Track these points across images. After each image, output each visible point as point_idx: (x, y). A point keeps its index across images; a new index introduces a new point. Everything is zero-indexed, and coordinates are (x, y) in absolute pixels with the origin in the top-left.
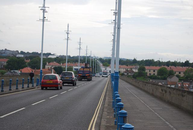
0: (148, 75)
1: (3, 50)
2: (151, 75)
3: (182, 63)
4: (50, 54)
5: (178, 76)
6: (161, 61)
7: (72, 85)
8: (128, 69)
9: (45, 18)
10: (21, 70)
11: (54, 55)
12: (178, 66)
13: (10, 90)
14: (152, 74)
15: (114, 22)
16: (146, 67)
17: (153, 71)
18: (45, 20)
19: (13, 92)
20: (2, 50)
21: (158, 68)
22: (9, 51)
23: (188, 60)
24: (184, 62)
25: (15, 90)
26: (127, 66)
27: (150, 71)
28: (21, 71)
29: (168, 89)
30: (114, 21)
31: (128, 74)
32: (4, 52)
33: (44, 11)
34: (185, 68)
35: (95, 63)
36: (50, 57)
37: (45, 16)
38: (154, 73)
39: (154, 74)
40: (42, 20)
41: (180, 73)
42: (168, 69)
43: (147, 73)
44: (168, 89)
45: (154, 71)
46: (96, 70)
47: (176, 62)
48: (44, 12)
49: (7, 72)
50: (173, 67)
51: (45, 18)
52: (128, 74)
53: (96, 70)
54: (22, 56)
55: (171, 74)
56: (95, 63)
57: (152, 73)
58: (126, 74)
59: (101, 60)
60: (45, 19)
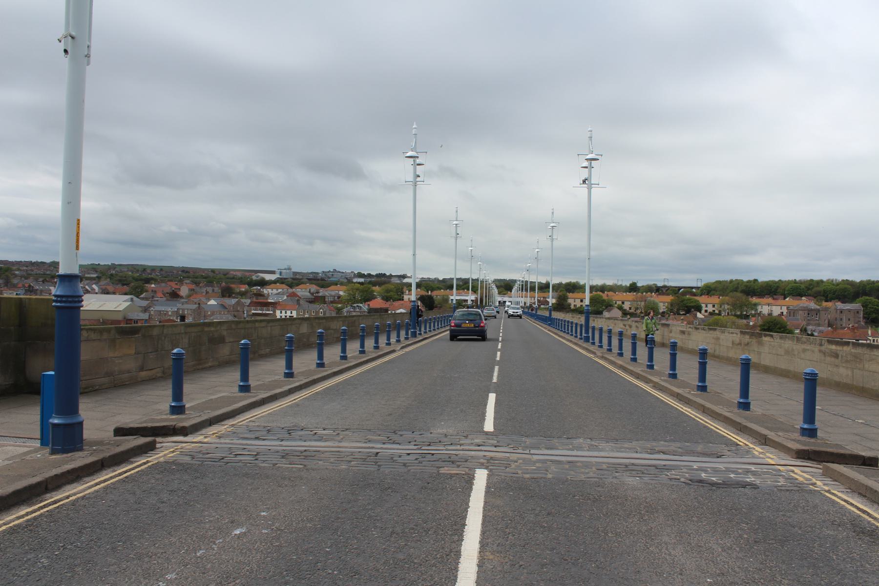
0: (572, 307)
1: (330, 272)
2: (577, 306)
5: (620, 308)
9: (458, 234)
14: (578, 306)
15: (550, 238)
17: (579, 300)
20: (328, 272)
22: (339, 272)
24: (628, 285)
27: (575, 302)
28: (369, 305)
29: (634, 323)
30: (550, 236)
33: (552, 240)
34: (631, 296)
37: (458, 233)
41: (623, 303)
42: (604, 296)
43: (570, 305)
44: (634, 323)
46: (489, 299)
47: (616, 285)
49: (347, 307)
50: (611, 293)
51: (458, 234)
53: (489, 299)
54: (362, 280)
55: (609, 306)
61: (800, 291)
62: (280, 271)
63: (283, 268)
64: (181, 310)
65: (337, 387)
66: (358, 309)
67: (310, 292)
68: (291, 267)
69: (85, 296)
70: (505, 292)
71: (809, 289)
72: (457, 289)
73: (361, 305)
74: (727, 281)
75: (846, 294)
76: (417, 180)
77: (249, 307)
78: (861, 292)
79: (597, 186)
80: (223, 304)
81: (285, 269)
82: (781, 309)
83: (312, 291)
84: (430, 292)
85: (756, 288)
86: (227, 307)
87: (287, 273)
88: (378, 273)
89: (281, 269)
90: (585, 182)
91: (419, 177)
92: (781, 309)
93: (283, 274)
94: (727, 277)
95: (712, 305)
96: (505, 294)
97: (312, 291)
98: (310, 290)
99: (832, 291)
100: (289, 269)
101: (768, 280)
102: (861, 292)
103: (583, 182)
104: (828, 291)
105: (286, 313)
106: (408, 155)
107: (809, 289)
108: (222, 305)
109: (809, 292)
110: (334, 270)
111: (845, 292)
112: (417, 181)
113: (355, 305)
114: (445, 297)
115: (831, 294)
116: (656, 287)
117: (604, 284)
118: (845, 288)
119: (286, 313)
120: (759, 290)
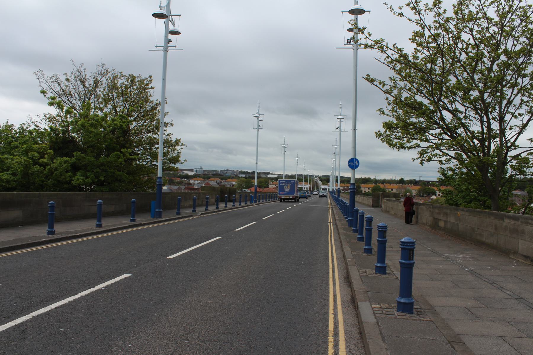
0: (363, 192)
1: (225, 170)
3: (397, 180)
4: (269, 173)
6: (377, 179)
7: (294, 201)
8: (346, 188)
9: (260, 126)
10: (250, 189)
11: (273, 174)
12: (387, 183)
13: (226, 207)
16: (362, 185)
18: (169, 48)
19: (248, 206)
21: (373, 185)
23: (403, 178)
25: (215, 210)
26: (345, 184)
28: (250, 190)
31: (345, 191)
32: (226, 172)
35: (315, 181)
36: (269, 176)
38: (369, 190)
39: (369, 191)
40: (162, 48)
42: (381, 186)
43: (362, 191)
45: (369, 189)
48: (258, 120)
51: (260, 126)
52: (345, 191)
56: (315, 181)
57: (367, 190)
58: (343, 192)
59: (320, 178)
60: (260, 127)
67: (216, 182)
87: (200, 171)
91: (171, 41)
93: (198, 172)
100: (201, 168)
108: (170, 189)
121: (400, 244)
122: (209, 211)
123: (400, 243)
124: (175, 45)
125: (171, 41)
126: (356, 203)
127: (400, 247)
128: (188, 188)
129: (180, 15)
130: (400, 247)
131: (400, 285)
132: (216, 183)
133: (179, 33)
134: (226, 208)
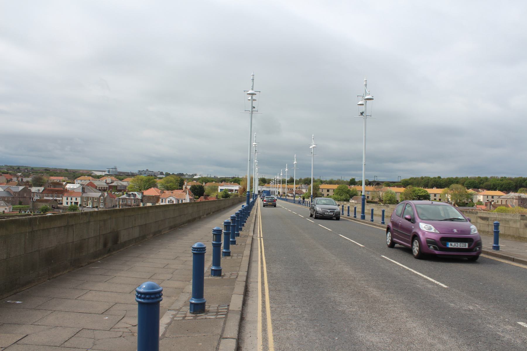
1: (143, 171)
20: (143, 171)
24: (349, 181)
25: (352, 217)
61: (475, 184)
62: (108, 170)
63: (111, 168)
64: (61, 199)
65: (503, 332)
66: (133, 196)
67: (106, 182)
68: (117, 167)
69: (377, 201)
70: (263, 184)
71: (480, 183)
72: (287, 183)
73: (136, 193)
74: (419, 178)
75: (510, 186)
76: (253, 110)
77: (42, 194)
78: (518, 185)
79: (370, 117)
80: (9, 191)
81: (112, 169)
82: (487, 198)
83: (107, 182)
84: (204, 183)
85: (442, 182)
86: (12, 194)
87: (113, 171)
88: (178, 173)
89: (109, 169)
90: (362, 114)
91: (255, 108)
92: (487, 198)
93: (110, 172)
94: (419, 176)
95: (360, 191)
96: (263, 186)
97: (107, 182)
98: (106, 181)
99: (500, 185)
100: (116, 169)
101: (518, 177)
102: (518, 185)
103: (361, 114)
104: (497, 185)
105: (71, 199)
106: (249, 92)
107: (480, 183)
108: (8, 191)
109: (481, 185)
110: (147, 170)
111: (510, 185)
112: (253, 111)
113: (131, 193)
114: (216, 187)
115: (499, 187)
116: (369, 182)
117: (332, 180)
118: (510, 183)
119: (71, 199)
120: (444, 184)
121: (213, 231)
122: (357, 219)
123: (213, 231)
124: (257, 110)
125: (255, 108)
126: (374, 215)
127: (213, 233)
128: (49, 190)
129: (260, 92)
130: (213, 233)
131: (204, 268)
132: (105, 184)
133: (256, 100)
134: (349, 217)
